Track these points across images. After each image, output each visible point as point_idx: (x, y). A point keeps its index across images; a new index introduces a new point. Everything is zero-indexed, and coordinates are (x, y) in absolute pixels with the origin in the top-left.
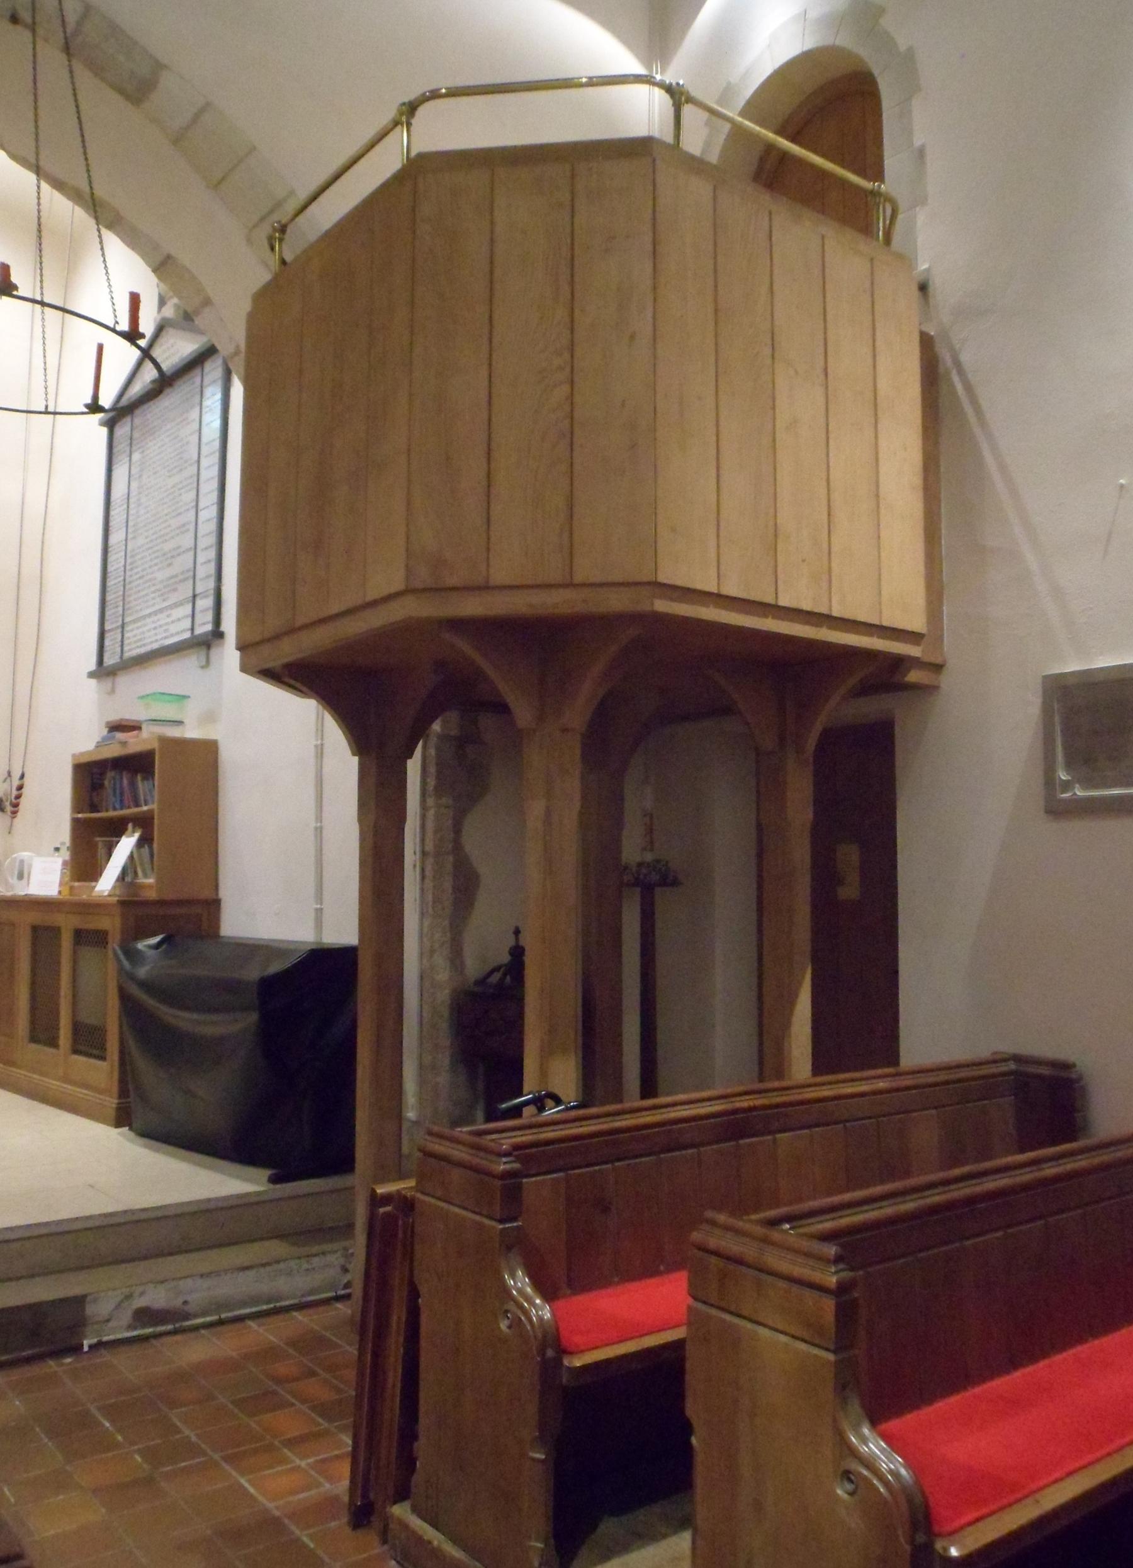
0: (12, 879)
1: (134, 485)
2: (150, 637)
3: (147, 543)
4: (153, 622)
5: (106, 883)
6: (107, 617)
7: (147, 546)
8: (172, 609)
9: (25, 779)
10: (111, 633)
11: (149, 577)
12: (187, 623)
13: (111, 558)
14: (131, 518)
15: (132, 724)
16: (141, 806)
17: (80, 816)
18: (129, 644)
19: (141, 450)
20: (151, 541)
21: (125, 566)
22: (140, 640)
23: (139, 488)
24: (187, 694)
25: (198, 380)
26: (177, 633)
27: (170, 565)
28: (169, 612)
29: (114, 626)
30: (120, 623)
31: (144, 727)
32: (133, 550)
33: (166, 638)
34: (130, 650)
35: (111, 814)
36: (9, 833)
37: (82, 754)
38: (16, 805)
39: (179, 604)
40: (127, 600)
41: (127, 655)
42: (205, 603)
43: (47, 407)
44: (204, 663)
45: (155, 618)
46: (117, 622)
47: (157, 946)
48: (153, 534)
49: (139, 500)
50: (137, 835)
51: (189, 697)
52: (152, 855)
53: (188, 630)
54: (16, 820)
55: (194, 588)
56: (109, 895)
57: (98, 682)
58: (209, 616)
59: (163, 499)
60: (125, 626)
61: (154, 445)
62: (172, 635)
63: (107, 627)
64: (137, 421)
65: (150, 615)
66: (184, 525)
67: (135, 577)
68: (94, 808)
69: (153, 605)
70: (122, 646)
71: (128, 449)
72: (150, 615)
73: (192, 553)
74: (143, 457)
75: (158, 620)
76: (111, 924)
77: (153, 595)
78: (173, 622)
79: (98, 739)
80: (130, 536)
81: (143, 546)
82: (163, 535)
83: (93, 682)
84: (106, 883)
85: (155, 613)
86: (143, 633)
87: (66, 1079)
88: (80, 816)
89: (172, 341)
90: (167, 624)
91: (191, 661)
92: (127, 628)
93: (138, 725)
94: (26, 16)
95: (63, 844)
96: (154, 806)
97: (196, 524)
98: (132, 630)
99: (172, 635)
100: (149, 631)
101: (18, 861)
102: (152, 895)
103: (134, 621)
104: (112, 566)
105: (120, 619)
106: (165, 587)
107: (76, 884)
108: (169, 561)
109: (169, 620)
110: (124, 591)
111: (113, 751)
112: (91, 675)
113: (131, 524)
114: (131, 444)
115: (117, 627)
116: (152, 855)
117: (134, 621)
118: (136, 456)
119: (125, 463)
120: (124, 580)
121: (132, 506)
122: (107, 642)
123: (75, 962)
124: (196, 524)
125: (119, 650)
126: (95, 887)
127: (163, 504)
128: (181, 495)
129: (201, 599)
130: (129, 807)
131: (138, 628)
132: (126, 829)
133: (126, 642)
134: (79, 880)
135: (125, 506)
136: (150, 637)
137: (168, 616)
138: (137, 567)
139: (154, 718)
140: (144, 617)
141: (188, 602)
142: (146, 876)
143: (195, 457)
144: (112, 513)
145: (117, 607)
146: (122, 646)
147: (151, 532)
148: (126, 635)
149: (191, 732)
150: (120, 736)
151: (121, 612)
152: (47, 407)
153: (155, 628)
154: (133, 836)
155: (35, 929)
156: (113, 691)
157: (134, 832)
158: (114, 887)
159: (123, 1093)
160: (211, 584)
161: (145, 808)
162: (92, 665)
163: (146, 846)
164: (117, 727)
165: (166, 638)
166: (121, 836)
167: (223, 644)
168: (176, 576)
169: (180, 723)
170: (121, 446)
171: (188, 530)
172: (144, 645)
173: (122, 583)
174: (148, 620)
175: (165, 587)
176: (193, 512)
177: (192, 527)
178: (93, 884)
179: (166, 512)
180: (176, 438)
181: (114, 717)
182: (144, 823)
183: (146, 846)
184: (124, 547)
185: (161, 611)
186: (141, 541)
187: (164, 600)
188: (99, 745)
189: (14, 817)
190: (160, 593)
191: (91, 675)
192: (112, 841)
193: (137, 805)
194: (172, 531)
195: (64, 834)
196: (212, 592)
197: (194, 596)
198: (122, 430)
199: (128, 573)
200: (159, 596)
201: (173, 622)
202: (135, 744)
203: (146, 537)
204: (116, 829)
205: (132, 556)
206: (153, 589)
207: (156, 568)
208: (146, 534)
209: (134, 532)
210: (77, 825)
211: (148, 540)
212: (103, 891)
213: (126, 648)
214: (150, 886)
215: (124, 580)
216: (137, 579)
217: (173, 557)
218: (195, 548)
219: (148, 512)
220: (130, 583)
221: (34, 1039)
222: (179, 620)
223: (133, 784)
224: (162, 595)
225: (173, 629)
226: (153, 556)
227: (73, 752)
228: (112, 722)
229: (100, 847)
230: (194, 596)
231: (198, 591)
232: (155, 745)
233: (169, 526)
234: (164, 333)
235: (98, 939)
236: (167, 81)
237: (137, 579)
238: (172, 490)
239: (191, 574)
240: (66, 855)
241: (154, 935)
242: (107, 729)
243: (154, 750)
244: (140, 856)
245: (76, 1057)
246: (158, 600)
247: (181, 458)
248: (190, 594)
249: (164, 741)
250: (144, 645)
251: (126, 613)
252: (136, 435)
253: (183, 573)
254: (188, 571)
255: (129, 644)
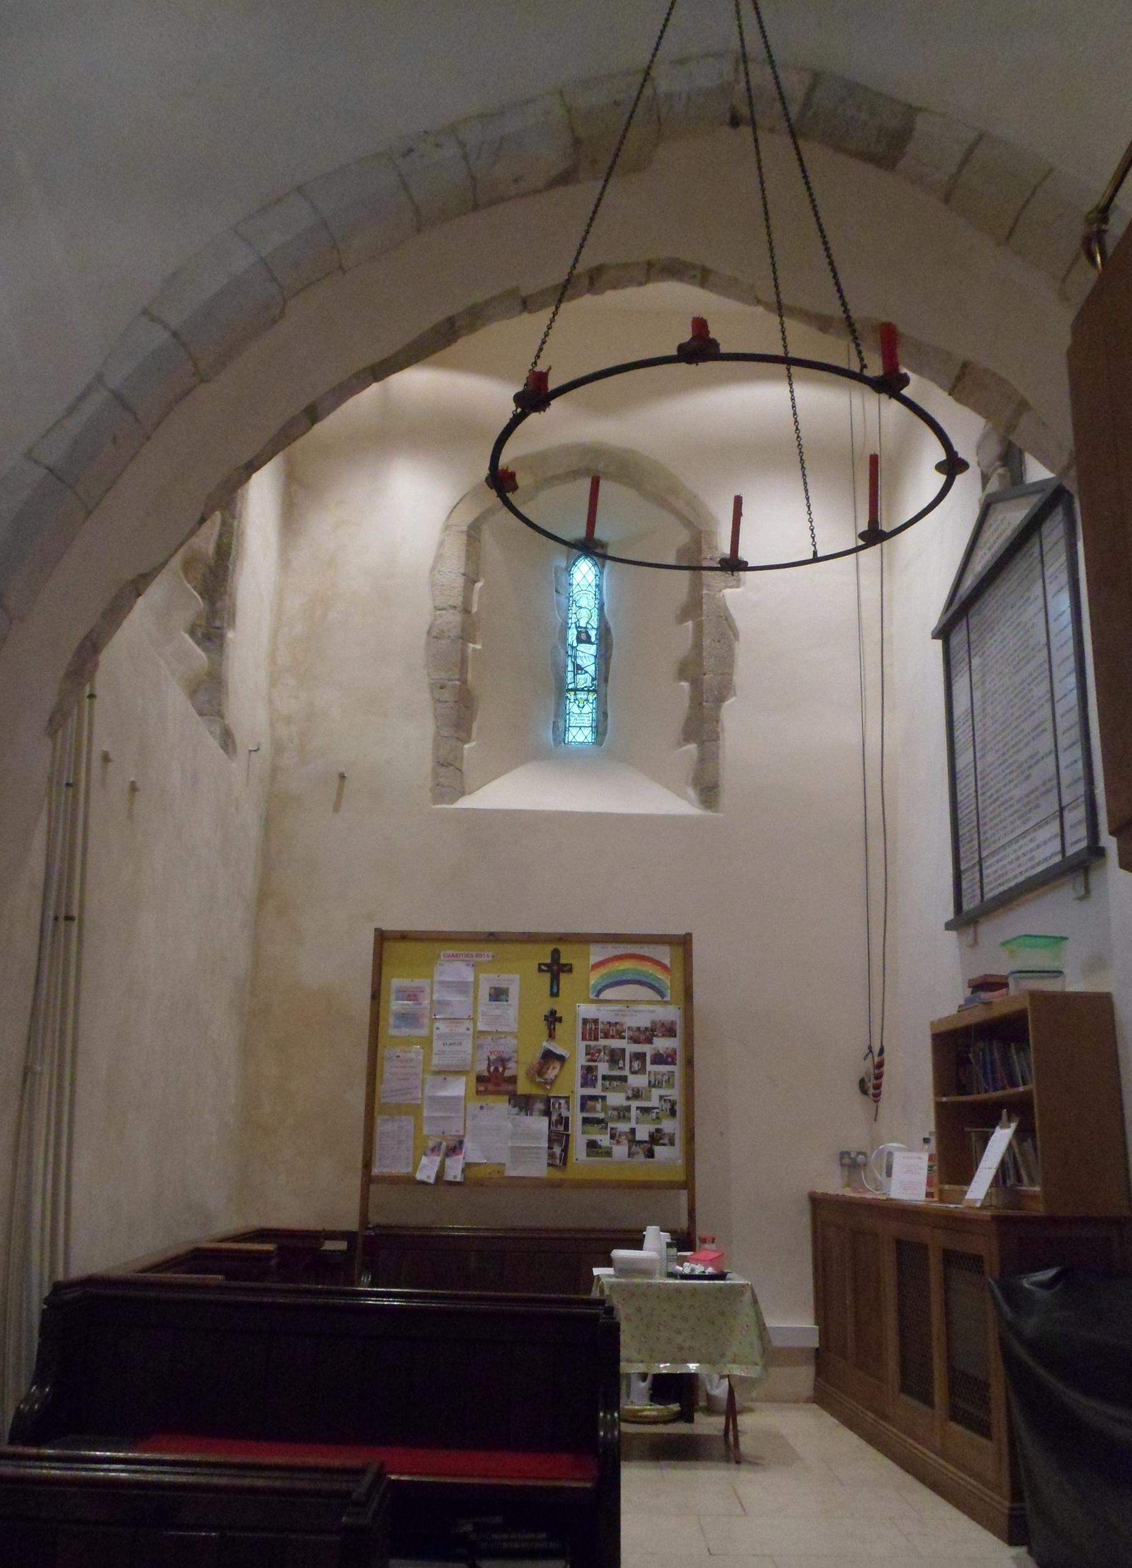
0: (881, 1175)
1: (977, 694)
2: (1013, 870)
3: (999, 758)
4: (1015, 851)
5: (979, 1188)
6: (962, 855)
7: (999, 762)
8: (1035, 831)
9: (885, 1054)
10: (968, 873)
11: (1006, 797)
12: (1056, 845)
13: (960, 785)
14: (977, 734)
15: (997, 980)
16: (1019, 1086)
17: (944, 1099)
18: (990, 883)
19: (980, 654)
20: (1003, 754)
21: (976, 791)
22: (1000, 876)
23: (983, 697)
24: (1064, 935)
25: (1036, 549)
26: (1045, 860)
27: (1027, 778)
28: (1032, 836)
29: (970, 864)
30: (977, 859)
31: (1011, 981)
32: (984, 770)
33: (1033, 867)
34: (991, 890)
35: (982, 1096)
36: (875, 1120)
37: (940, 1021)
38: (878, 1087)
39: (1045, 822)
40: (982, 829)
41: (989, 895)
42: (1077, 814)
43: (815, 553)
44: (1082, 892)
45: (1015, 847)
46: (973, 858)
47: (1049, 1285)
48: (1004, 746)
49: (984, 710)
50: (1013, 1126)
51: (1067, 938)
52: (1035, 1149)
53: (1058, 853)
54: (880, 1103)
55: (1060, 800)
56: (983, 1207)
57: (959, 934)
58: (1082, 831)
59: (1011, 700)
60: (983, 861)
61: (995, 641)
62: (1039, 864)
63: (963, 866)
64: (974, 621)
65: (1009, 843)
66: (1039, 725)
67: (988, 802)
68: (962, 1090)
69: (1013, 830)
70: (982, 888)
71: (966, 655)
72: (1009, 843)
73: (1053, 756)
74: (984, 660)
75: (1021, 847)
76: (986, 1247)
77: (1012, 819)
78: (1038, 847)
79: (962, 1002)
80: (978, 755)
81: (993, 763)
82: (1016, 744)
83: (953, 934)
84: (979, 1188)
85: (1016, 840)
86: (1004, 867)
87: (943, 1453)
88: (944, 1099)
89: (1000, 517)
90: (1031, 850)
91: (1065, 894)
92: (985, 865)
93: (1004, 981)
94: (744, 111)
95: (931, 1133)
96: (1032, 1086)
97: (1054, 720)
98: (990, 866)
99: (1039, 864)
100: (1010, 863)
101: (886, 1153)
102: (1038, 1209)
103: (993, 854)
104: (962, 794)
105: (976, 855)
106: (1024, 806)
107: (947, 1187)
108: (1027, 773)
109: (1033, 845)
110: (978, 821)
111: (978, 1015)
112: (949, 926)
113: (978, 740)
114: (969, 650)
115: (974, 865)
116: (1035, 1149)
117: (993, 854)
118: (976, 661)
119: (965, 673)
120: (977, 808)
121: (977, 719)
122: (965, 885)
123: (947, 1288)
124: (1054, 720)
125: (978, 891)
126: (965, 1193)
127: (1012, 707)
128: (1031, 690)
129: (1070, 810)
130: (1004, 1088)
131: (998, 862)
132: (999, 1118)
133: (985, 881)
134: (949, 1183)
135: (970, 722)
136: (1013, 870)
137: (1032, 840)
138: (989, 790)
139: (1020, 969)
140: (1004, 847)
141: (1054, 819)
142: (1032, 1182)
143: (1044, 640)
144: (956, 734)
145: (972, 840)
146: (982, 888)
147: (1001, 745)
148: (985, 872)
149: (1075, 984)
150: (985, 996)
151: (977, 847)
152: (815, 553)
153: (1018, 858)
154: (1009, 1127)
155: (900, 1244)
156: (975, 942)
157: (1009, 1121)
158: (988, 1194)
159: (1017, 1495)
160: (1081, 788)
161: (1021, 1089)
162: (950, 915)
163: (1029, 1139)
164: (984, 985)
165: (1033, 867)
166: (994, 1127)
167: (1105, 863)
168: (1037, 789)
169: (1059, 973)
170: (959, 654)
171: (1045, 730)
172: (1008, 881)
173: (975, 812)
174: (1009, 850)
175: (1024, 806)
176: (1048, 706)
177: (1049, 725)
178: (965, 1188)
179: (1017, 714)
180: (1018, 625)
181: (978, 973)
182: (1021, 1109)
183: (1029, 1139)
184: (973, 770)
185: (1024, 834)
186: (990, 758)
187: (1024, 823)
188: (961, 1009)
189: (878, 1101)
190: (1019, 814)
191: (949, 926)
192: (988, 1132)
193: (1014, 1085)
194: (1026, 736)
195: (925, 1120)
196: (1083, 799)
197: (1062, 809)
198: (958, 638)
199: (980, 799)
200: (1019, 819)
201: (1038, 847)
202: (1002, 1003)
203: (997, 751)
204: (988, 1119)
205: (982, 779)
206: (1010, 811)
207: (1012, 785)
208: (997, 748)
209: (982, 749)
210: (941, 1110)
211: (1000, 753)
212: (976, 1200)
213: (986, 889)
214: (1033, 1197)
215: (977, 808)
216: (990, 804)
217: (1030, 767)
218: (1056, 751)
219: (996, 721)
220: (984, 809)
221: (905, 1388)
222: (1045, 843)
223: (1006, 1059)
224: (1022, 816)
225: (1040, 855)
226: (1007, 771)
227: (932, 1019)
228: (973, 980)
229: (974, 1139)
230: (1062, 809)
231: (1065, 802)
232: (1027, 1004)
233: (1022, 731)
234: (991, 511)
235: (975, 1263)
236: (921, 124)
237: (990, 804)
238: (1022, 687)
239: (1055, 782)
240: (933, 1146)
241: (1046, 1267)
242: (970, 989)
243: (1025, 1011)
244: (1023, 1154)
245: (954, 1426)
246: (1018, 822)
247: (1027, 647)
248: (1057, 808)
249: (1037, 997)
250: (1008, 881)
251: (983, 845)
252: (973, 637)
253: (1044, 784)
254: (1050, 780)
255: (990, 883)
